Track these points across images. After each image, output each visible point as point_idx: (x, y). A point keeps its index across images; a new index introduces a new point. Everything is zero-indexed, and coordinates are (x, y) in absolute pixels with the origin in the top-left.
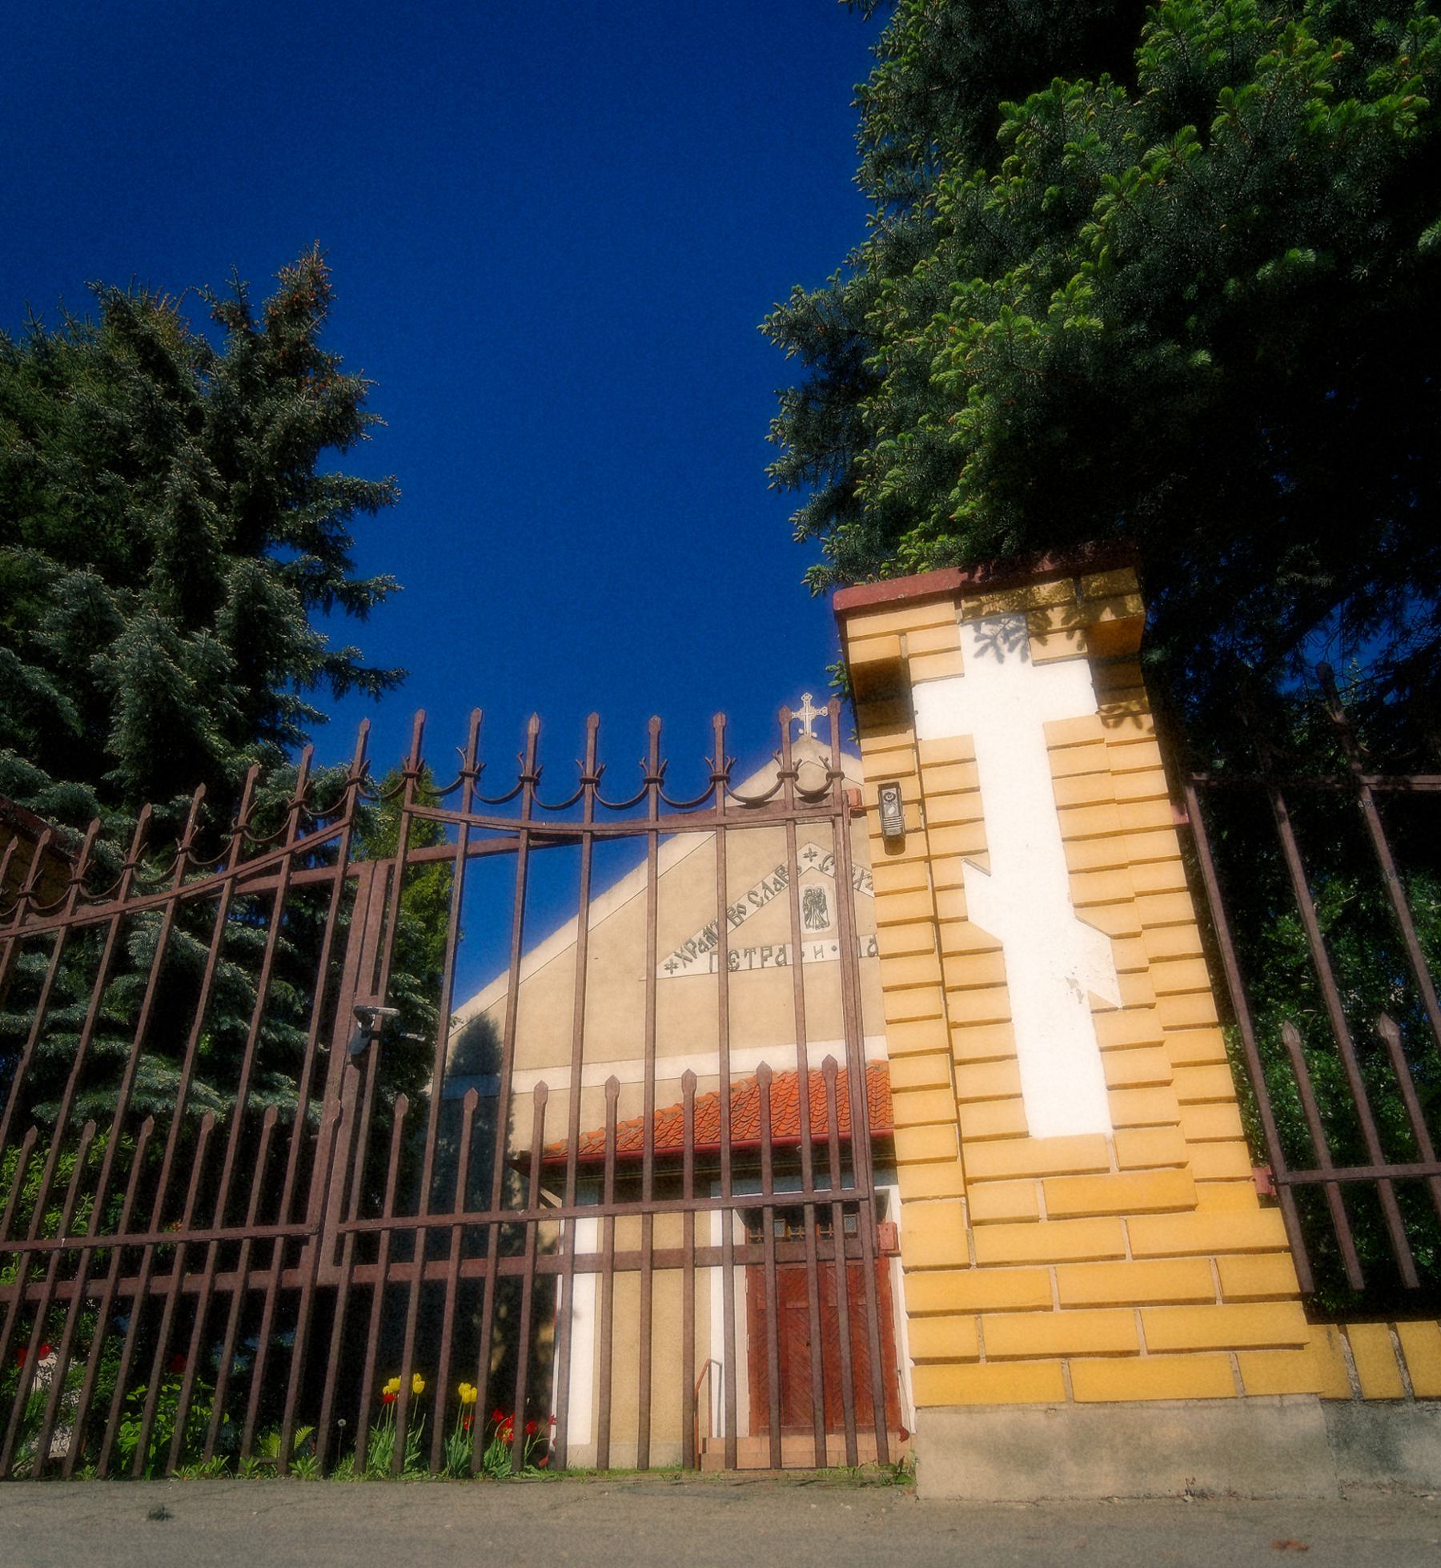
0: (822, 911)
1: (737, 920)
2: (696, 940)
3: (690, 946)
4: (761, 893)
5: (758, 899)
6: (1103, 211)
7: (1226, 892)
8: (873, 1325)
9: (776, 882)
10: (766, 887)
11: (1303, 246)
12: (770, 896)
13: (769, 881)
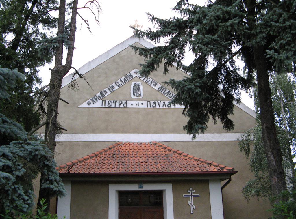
0: (138, 91)
1: (112, 91)
2: (98, 95)
3: (96, 97)
4: (120, 83)
5: (118, 84)
6: (41, 108)
7: (167, 174)
8: (125, 206)
9: (125, 80)
10: (121, 81)
11: (138, 110)
12: (123, 84)
13: (123, 79)
